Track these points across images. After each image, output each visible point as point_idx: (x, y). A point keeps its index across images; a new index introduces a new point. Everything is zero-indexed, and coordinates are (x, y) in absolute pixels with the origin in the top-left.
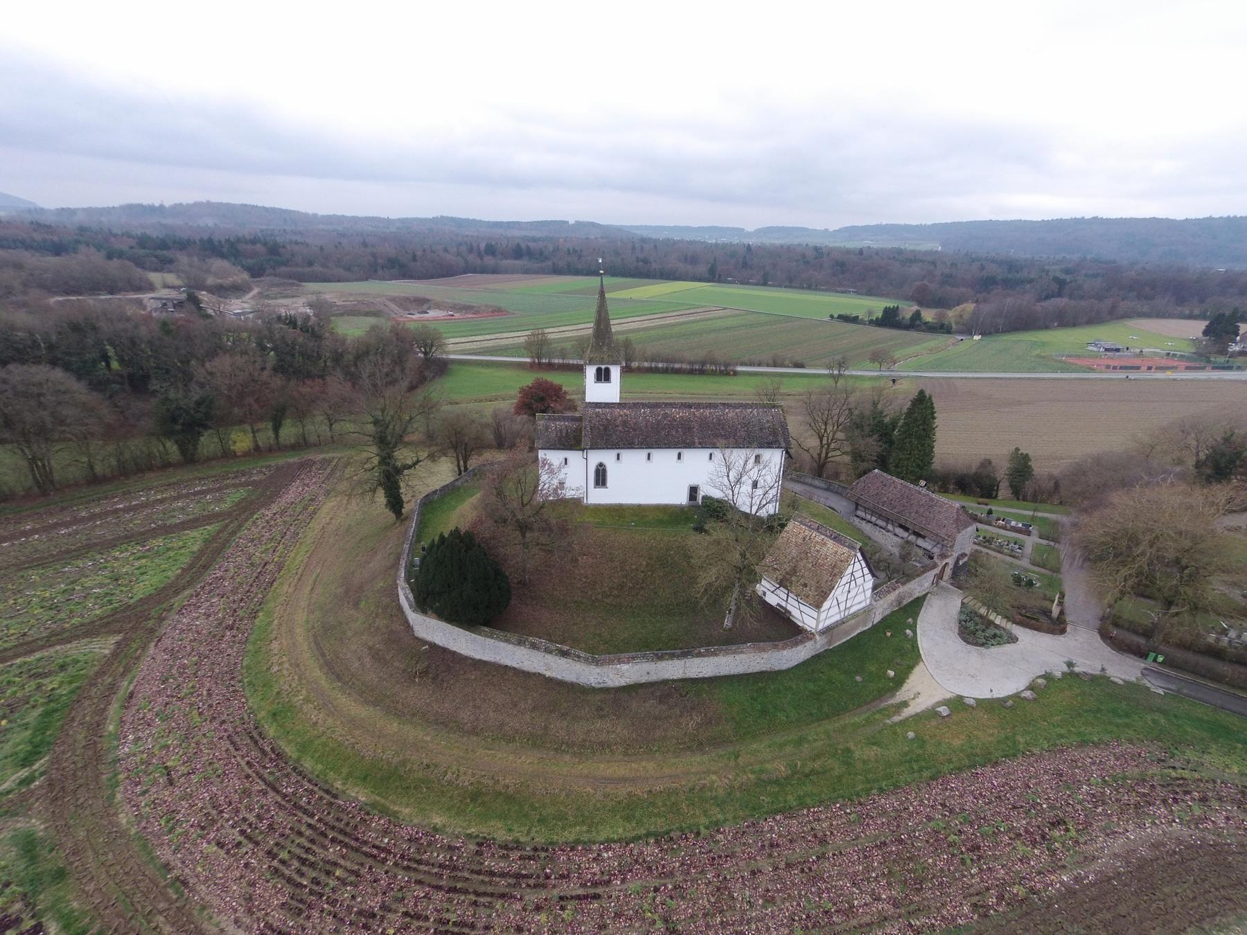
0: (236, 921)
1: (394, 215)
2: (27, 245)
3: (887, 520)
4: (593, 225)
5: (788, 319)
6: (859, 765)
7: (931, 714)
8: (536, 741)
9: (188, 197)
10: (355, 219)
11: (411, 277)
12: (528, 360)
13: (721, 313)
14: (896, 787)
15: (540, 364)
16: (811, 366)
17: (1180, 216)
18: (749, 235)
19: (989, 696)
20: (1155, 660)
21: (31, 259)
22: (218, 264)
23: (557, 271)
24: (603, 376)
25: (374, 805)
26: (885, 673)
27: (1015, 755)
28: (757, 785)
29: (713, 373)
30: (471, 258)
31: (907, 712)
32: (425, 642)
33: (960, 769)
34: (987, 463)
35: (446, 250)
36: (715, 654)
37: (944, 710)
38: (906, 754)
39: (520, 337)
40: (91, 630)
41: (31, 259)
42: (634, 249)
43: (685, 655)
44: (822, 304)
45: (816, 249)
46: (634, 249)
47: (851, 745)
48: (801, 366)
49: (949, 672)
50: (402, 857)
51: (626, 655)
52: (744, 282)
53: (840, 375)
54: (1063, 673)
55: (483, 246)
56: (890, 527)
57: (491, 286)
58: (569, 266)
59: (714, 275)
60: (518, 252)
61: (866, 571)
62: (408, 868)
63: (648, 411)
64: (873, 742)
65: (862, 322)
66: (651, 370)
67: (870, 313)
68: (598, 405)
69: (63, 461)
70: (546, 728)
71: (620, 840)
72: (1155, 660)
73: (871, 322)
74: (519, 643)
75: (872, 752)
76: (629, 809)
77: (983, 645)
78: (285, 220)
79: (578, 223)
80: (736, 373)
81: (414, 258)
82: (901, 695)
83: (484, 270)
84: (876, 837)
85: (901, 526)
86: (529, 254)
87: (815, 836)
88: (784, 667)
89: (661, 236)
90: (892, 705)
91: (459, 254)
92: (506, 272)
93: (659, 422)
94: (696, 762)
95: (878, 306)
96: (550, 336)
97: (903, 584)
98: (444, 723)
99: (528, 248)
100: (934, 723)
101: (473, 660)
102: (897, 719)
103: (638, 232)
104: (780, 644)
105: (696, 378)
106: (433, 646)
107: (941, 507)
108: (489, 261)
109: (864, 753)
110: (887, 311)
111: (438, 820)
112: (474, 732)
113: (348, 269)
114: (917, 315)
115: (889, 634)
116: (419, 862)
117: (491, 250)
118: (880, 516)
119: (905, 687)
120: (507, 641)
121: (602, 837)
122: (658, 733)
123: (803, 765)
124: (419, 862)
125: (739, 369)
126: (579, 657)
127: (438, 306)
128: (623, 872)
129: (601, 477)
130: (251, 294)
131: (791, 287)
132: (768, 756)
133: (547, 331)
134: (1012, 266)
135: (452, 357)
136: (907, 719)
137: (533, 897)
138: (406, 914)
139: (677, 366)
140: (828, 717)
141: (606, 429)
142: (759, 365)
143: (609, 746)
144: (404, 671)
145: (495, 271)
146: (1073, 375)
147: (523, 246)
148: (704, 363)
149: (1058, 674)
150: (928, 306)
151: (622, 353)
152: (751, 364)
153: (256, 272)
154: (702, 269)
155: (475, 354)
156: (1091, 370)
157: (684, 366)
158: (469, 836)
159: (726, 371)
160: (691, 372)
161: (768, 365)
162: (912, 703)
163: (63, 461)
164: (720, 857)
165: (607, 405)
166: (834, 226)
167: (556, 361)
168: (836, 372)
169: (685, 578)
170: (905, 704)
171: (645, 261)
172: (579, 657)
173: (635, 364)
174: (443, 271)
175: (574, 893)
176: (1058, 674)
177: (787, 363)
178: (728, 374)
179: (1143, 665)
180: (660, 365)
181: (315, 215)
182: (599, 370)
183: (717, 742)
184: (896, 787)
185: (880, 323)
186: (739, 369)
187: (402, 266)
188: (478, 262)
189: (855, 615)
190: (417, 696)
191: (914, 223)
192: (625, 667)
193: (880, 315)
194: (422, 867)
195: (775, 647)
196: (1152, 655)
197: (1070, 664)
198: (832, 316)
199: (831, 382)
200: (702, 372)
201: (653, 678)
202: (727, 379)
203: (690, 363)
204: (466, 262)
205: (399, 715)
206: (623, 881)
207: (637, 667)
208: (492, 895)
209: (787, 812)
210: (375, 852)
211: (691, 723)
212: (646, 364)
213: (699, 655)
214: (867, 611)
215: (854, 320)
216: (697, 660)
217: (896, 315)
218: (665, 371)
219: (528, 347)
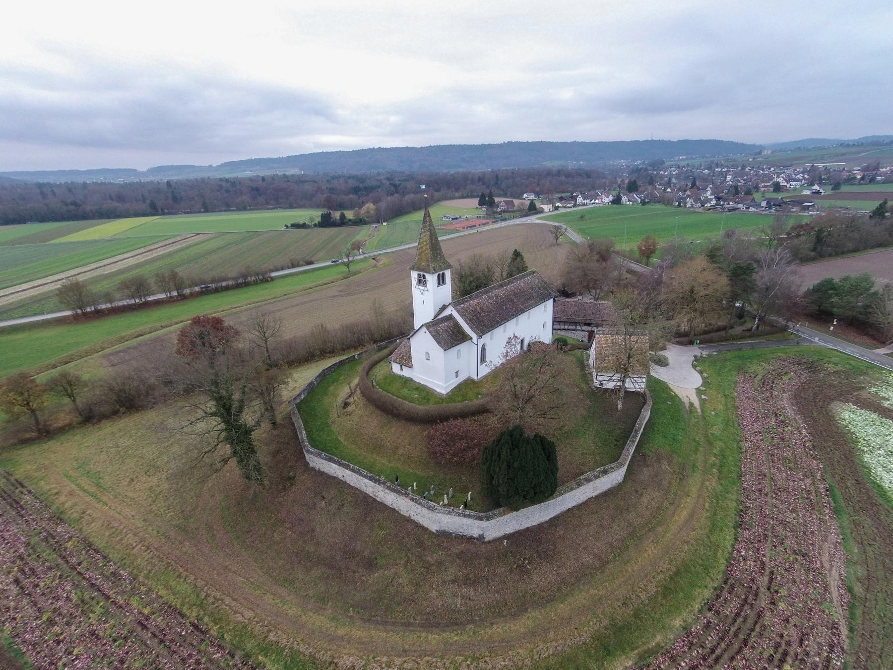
3: (576, 324)
5: (257, 234)
12: (68, 313)
16: (319, 261)
17: (418, 145)
18: (142, 173)
25: (641, 657)
29: (255, 283)
32: (500, 540)
44: (275, 219)
45: (40, 186)
48: (311, 263)
50: (705, 659)
56: (578, 328)
59: (154, 210)
62: (717, 660)
65: (309, 227)
73: (315, 225)
74: (579, 485)
80: (272, 279)
85: (586, 324)
98: (583, 575)
101: (546, 522)
105: (245, 289)
106: (507, 537)
111: (678, 622)
112: (604, 564)
114: (343, 216)
116: (713, 651)
118: (571, 323)
120: (572, 489)
121: (730, 549)
122: (665, 483)
124: (713, 651)
125: (274, 274)
126: (612, 468)
131: (229, 211)
134: (361, 179)
137: (763, 601)
139: (224, 284)
142: (282, 269)
144: (511, 571)
146: (455, 235)
148: (245, 276)
150: (336, 210)
151: (172, 285)
156: (458, 231)
157: (230, 283)
158: (700, 611)
159: (264, 279)
160: (238, 286)
166: (217, 161)
167: (103, 307)
170: (691, 404)
171: (74, 204)
172: (612, 468)
173: (187, 291)
178: (267, 281)
186: (274, 274)
190: (541, 577)
191: (275, 157)
193: (320, 219)
194: (718, 651)
198: (287, 226)
200: (246, 284)
202: (266, 285)
203: (234, 279)
205: (551, 599)
206: (764, 556)
208: (756, 623)
212: (197, 289)
215: (304, 226)
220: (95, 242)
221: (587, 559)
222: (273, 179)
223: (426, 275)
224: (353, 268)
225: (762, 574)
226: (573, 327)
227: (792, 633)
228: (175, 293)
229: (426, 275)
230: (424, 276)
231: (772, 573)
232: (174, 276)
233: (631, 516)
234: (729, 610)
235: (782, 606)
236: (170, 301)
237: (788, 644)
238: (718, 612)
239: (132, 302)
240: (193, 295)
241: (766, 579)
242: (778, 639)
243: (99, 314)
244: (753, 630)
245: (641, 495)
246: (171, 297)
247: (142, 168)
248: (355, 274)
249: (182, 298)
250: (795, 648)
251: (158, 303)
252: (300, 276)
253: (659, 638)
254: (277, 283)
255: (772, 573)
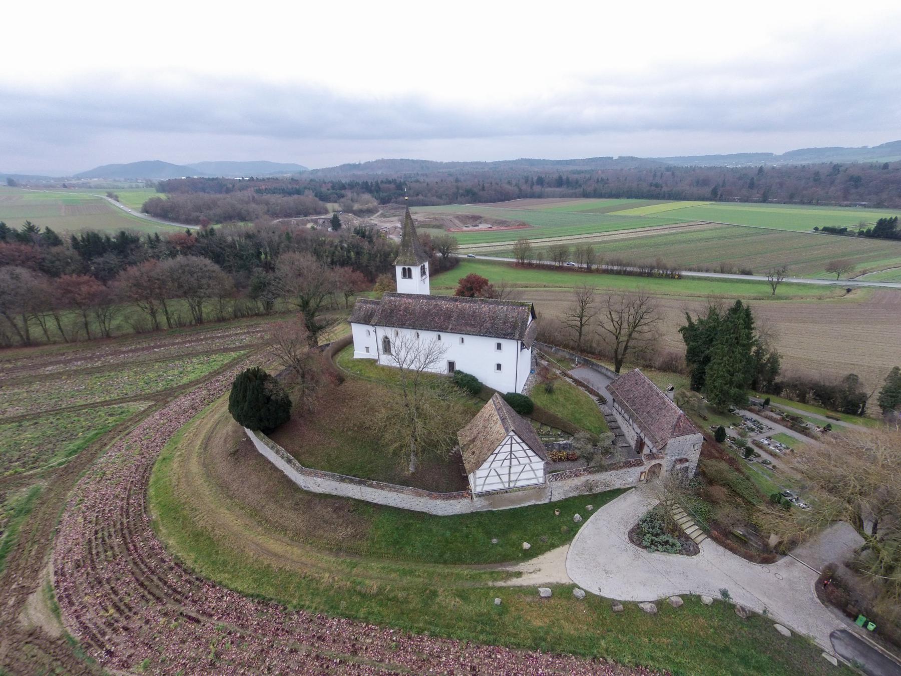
0: (55, 560)
1: (490, 159)
2: (274, 192)
4: (632, 159)
5: (769, 231)
6: (435, 608)
7: (533, 591)
8: (255, 513)
9: (371, 157)
10: (465, 164)
11: (479, 202)
12: (515, 260)
13: (705, 227)
14: (449, 637)
15: (523, 264)
18: (777, 158)
19: (597, 593)
20: (865, 625)
21: (274, 199)
22: (367, 196)
23: (585, 195)
24: (407, 274)
26: (521, 544)
27: (584, 655)
28: (349, 591)
29: (660, 276)
30: (524, 187)
31: (515, 582)
33: (518, 646)
34: (852, 379)
35: (509, 183)
36: (382, 488)
37: (545, 592)
38: (482, 615)
39: (510, 245)
40: (137, 398)
41: (274, 199)
42: (655, 176)
43: (360, 483)
46: (655, 176)
47: (440, 590)
48: (749, 273)
49: (601, 563)
51: (323, 472)
52: (745, 200)
53: (778, 283)
54: (715, 600)
55: (535, 179)
57: (530, 207)
58: (595, 190)
60: (559, 182)
61: (530, 453)
63: (425, 301)
64: (462, 595)
65: (851, 234)
66: (606, 272)
67: (861, 226)
68: (409, 296)
69: (208, 309)
70: (263, 507)
71: (240, 593)
72: (865, 625)
73: (861, 234)
74: (272, 448)
75: (453, 602)
76: (263, 574)
77: (645, 547)
78: (422, 168)
79: (621, 158)
81: (483, 189)
82: (522, 567)
83: (532, 196)
84: (397, 667)
86: (577, 184)
87: (353, 645)
88: (440, 514)
89: (688, 165)
90: (507, 572)
91: (517, 185)
92: (548, 197)
93: (429, 310)
94: (327, 559)
95: (872, 217)
96: (533, 245)
97: (590, 473)
99: (568, 179)
100: (529, 599)
102: (501, 584)
103: (671, 162)
104: (435, 494)
107: (668, 411)
108: (537, 189)
109: (447, 601)
110: (881, 223)
111: (171, 542)
113: (440, 197)
115: (557, 513)
117: (541, 181)
119: (534, 561)
120: (267, 445)
121: (232, 586)
122: (321, 532)
123: (391, 591)
125: (684, 273)
127: (486, 221)
128: (226, 613)
129: (387, 345)
130: (379, 213)
132: (374, 575)
133: (529, 241)
135: (460, 256)
136: (509, 587)
137: (170, 606)
138: (112, 588)
139: (629, 269)
140: (445, 562)
141: (392, 311)
142: (707, 271)
143: (286, 530)
145: (540, 196)
147: (564, 178)
148: (652, 268)
149: (707, 599)
151: (585, 258)
152: (699, 270)
153: (384, 201)
154: (707, 191)
155: (485, 255)
159: (672, 275)
160: (641, 275)
161: (715, 272)
162: (524, 577)
163: (208, 309)
164: (283, 630)
165: (419, 297)
167: (535, 262)
168: (775, 279)
169: (432, 433)
170: (519, 574)
171: (657, 186)
172: (295, 465)
173: (594, 267)
174: (502, 197)
175: (190, 614)
176: (707, 599)
177: (735, 269)
178: (673, 277)
179: (843, 626)
180: (615, 268)
181: (441, 163)
182: (404, 269)
183: (352, 552)
184: (449, 637)
185: (870, 235)
187: (474, 194)
188: (529, 190)
189: (522, 488)
192: (320, 480)
193: (873, 227)
195: (430, 496)
196: (862, 619)
197: (725, 593)
199: (768, 289)
200: (650, 275)
201: (340, 493)
204: (520, 190)
206: (219, 619)
207: (328, 482)
209: (352, 619)
210: (132, 548)
211: (343, 533)
212: (604, 267)
213: (371, 486)
214: (539, 489)
215: (842, 232)
216: (369, 489)
217: (892, 227)
218: (619, 273)
219: (516, 252)
220: (631, 217)
221: (234, 486)
222: (694, 170)
223: (412, 268)
224: (780, 290)
225: (198, 611)
226: (627, 417)
227: (136, 623)
228: (585, 266)
229: (412, 268)
230: (409, 269)
231: (198, 621)
232: (590, 252)
233: (271, 506)
234: (171, 578)
235: (162, 620)
236: (580, 270)
237: (128, 618)
238: (171, 569)
239: (553, 263)
240: (598, 271)
241: (194, 615)
242: (134, 610)
243: (530, 266)
244: (150, 593)
245: (295, 510)
246: (581, 268)
247: (779, 152)
248: (779, 298)
249: (589, 271)
250: (123, 622)
251: (570, 270)
252: (696, 282)
253: (164, 531)
254: (681, 283)
255: (198, 621)
